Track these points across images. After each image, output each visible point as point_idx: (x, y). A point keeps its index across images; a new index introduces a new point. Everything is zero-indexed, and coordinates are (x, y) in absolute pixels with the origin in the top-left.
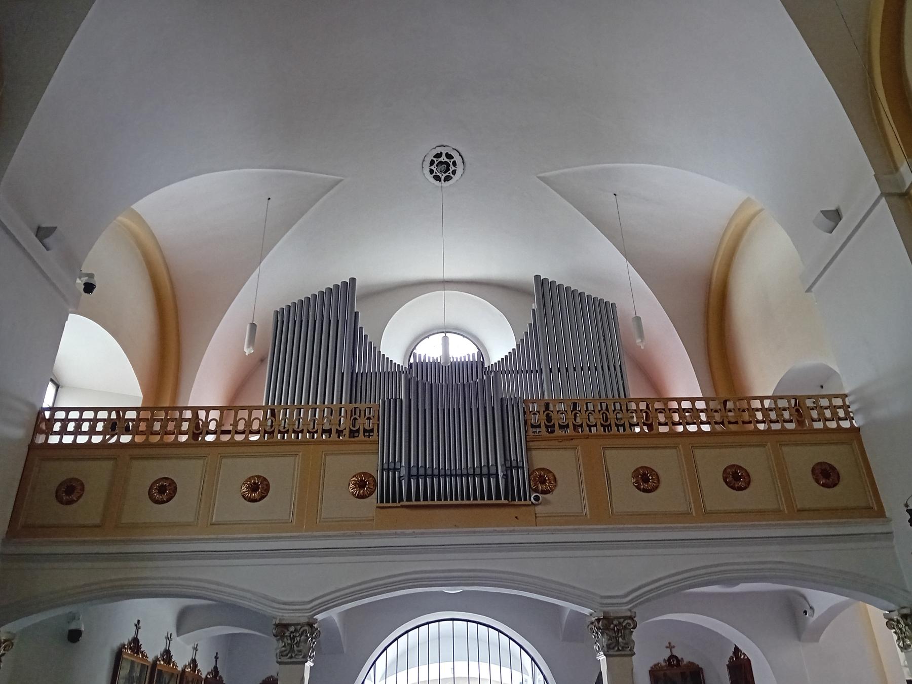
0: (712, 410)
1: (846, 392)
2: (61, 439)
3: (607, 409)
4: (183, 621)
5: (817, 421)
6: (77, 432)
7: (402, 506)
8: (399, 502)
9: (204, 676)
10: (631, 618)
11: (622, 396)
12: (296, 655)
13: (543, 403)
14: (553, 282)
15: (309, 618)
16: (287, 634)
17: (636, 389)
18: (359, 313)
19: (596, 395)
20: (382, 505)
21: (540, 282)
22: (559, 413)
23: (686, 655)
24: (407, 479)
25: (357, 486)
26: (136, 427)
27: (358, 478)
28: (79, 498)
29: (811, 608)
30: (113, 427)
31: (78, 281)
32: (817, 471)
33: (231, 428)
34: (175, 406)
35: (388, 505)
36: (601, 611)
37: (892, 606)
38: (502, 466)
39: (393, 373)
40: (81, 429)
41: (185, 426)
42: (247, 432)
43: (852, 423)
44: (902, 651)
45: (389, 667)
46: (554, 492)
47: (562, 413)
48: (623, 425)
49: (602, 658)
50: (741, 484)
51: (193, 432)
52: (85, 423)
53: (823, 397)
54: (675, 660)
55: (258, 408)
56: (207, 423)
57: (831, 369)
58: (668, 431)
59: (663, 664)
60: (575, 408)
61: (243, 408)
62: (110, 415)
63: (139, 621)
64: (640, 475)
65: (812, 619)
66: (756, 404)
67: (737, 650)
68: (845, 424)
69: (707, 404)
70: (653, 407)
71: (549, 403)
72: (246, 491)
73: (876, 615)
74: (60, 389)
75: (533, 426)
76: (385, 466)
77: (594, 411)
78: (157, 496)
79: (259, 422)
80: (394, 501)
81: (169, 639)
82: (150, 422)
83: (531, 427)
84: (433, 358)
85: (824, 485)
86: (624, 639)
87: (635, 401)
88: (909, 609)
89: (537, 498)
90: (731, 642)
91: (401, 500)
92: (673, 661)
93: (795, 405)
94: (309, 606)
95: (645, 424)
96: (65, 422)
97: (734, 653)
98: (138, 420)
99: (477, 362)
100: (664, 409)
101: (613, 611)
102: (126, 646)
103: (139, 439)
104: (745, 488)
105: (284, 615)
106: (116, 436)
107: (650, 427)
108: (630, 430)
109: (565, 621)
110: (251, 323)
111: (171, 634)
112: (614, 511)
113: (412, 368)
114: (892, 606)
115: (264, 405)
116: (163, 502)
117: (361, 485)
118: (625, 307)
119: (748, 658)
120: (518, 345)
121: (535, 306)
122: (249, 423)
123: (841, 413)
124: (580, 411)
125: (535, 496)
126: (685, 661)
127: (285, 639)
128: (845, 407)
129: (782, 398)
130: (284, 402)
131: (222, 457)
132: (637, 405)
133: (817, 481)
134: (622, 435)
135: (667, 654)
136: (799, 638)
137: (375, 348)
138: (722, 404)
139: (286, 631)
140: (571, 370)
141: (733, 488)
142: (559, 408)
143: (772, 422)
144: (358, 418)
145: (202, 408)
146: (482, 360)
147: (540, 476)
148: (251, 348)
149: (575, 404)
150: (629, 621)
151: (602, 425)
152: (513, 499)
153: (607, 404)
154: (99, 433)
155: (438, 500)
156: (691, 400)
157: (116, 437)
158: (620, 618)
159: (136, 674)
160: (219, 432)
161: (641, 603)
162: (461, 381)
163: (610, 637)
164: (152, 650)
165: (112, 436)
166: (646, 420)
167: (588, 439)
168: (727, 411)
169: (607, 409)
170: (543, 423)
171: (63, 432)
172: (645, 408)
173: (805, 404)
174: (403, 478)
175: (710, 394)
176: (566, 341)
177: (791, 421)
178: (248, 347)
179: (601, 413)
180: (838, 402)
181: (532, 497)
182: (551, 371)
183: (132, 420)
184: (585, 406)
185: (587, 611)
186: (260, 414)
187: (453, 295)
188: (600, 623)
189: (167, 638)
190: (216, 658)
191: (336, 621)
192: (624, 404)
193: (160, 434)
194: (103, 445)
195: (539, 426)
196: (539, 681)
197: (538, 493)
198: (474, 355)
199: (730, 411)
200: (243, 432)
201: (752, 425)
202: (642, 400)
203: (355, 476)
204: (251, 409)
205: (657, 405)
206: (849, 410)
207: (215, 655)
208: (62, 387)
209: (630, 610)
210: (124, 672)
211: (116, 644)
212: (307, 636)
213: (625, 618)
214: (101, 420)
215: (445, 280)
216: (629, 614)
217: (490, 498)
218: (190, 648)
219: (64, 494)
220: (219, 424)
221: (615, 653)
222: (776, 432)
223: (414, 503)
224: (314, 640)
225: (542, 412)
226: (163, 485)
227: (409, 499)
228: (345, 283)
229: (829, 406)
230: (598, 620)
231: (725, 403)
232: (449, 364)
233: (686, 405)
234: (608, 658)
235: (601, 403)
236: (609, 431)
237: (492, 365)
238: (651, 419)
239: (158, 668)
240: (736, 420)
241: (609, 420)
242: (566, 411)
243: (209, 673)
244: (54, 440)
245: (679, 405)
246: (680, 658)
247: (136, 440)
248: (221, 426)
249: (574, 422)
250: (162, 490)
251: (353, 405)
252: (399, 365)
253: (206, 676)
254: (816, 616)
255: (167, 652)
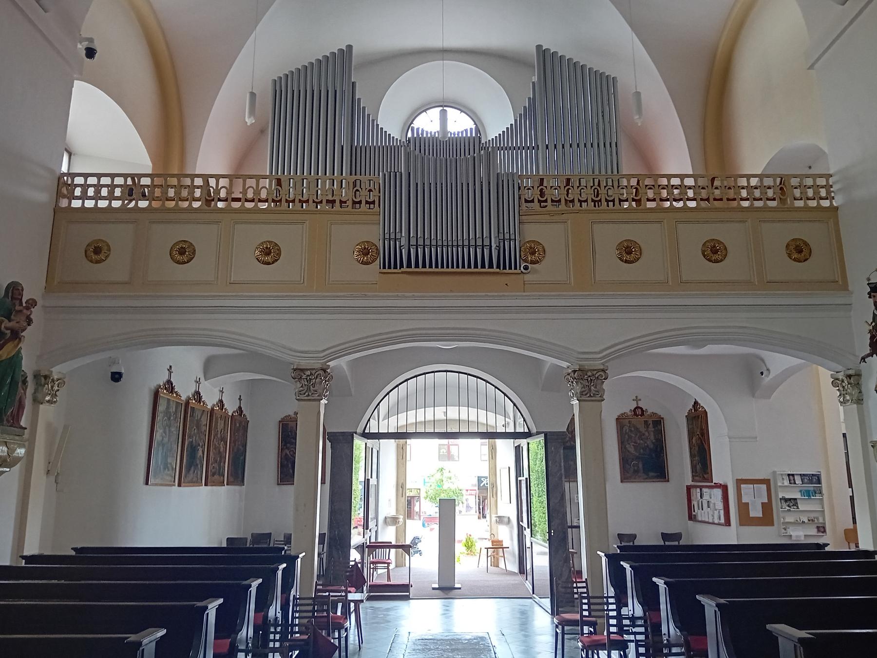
0: (699, 186)
1: (831, 172)
2: (83, 203)
3: (599, 185)
4: (210, 368)
5: (798, 200)
6: (97, 197)
7: (402, 273)
8: (400, 269)
9: (230, 414)
10: (603, 370)
11: (615, 172)
12: (313, 394)
13: (537, 179)
14: (555, 53)
15: (322, 365)
16: (304, 377)
17: (629, 166)
18: (357, 84)
19: (590, 170)
20: (384, 271)
21: (542, 53)
22: (553, 188)
23: (650, 407)
24: (407, 248)
25: (361, 253)
26: (152, 192)
27: (362, 247)
28: (107, 257)
29: (768, 370)
30: (130, 193)
31: (79, 46)
32: (791, 247)
33: (240, 196)
34: (184, 173)
35: (389, 271)
36: (577, 364)
37: (840, 368)
38: (495, 238)
39: (391, 150)
40: (100, 194)
41: (198, 193)
42: (256, 200)
43: (831, 203)
44: (841, 405)
45: (391, 409)
46: (543, 263)
47: (556, 189)
48: (613, 201)
49: (575, 402)
50: (714, 257)
51: (206, 198)
52: (77, 188)
53: (808, 176)
54: (640, 410)
55: (265, 177)
56: (217, 191)
57: (821, 150)
58: (655, 206)
59: (629, 413)
60: (568, 184)
61: (251, 177)
62: (126, 181)
63: (171, 367)
64: (624, 247)
65: (767, 380)
66: (743, 182)
67: (696, 403)
68: (826, 203)
69: (696, 181)
70: (643, 183)
71: (543, 179)
72: (260, 255)
73: (825, 375)
74: (72, 157)
75: (526, 201)
76: (387, 236)
77: (586, 187)
78: (179, 258)
79: (266, 191)
80: (395, 267)
81: (198, 382)
82: (165, 187)
83: (525, 202)
84: (431, 133)
85: (795, 260)
86: (596, 387)
87: (666, 176)
88: (854, 370)
89: (526, 268)
90: (692, 397)
91: (402, 266)
92: (639, 411)
93: (781, 184)
94: (322, 355)
95: (633, 200)
96: (85, 187)
97: (694, 406)
98: (153, 186)
99: (474, 137)
100: (653, 186)
101: (587, 364)
102: (162, 387)
103: (156, 204)
104: (721, 261)
105: (301, 361)
106: (134, 202)
107: (638, 202)
108: (619, 206)
109: (546, 370)
110: (250, 92)
111: (199, 379)
112: (597, 280)
113: (410, 143)
114: (840, 368)
115: (268, 174)
116: (184, 263)
117: (365, 252)
118: (626, 80)
119: (705, 410)
120: (516, 121)
121: (535, 79)
122: (257, 192)
123: (823, 192)
124: (573, 187)
125: (524, 266)
126: (650, 411)
127: (303, 382)
128: (828, 187)
129: (768, 176)
130: (287, 172)
131: (236, 223)
132: (629, 181)
133: (790, 256)
134: (612, 210)
135: (634, 405)
136: (753, 396)
137: (373, 121)
138: (710, 181)
139: (303, 375)
140: (567, 146)
141: (710, 260)
142: (552, 182)
143: (755, 199)
144: (360, 189)
145: (212, 176)
146: (479, 135)
147: (531, 248)
148: (252, 118)
149: (568, 180)
150: (602, 373)
151: (593, 200)
152: (505, 268)
153: (599, 180)
154: (117, 198)
155: (436, 267)
156: (666, 176)
157: (134, 202)
158: (594, 370)
159: (173, 409)
160: (229, 199)
161: (612, 359)
162: (455, 156)
163: (584, 386)
164: (185, 391)
165: (131, 201)
166: (636, 196)
167: (578, 214)
168: (714, 188)
169: (599, 185)
170: (537, 196)
171: (84, 197)
172: (635, 184)
173: (790, 183)
174: (403, 247)
175: (701, 172)
176: (572, 112)
177: (774, 199)
178: (249, 117)
179: (593, 188)
180: (822, 182)
181: (522, 266)
182: (547, 147)
183: (148, 186)
184: (605, 182)
185: (565, 364)
186: (266, 183)
187: (451, 65)
188: (576, 374)
189: (196, 382)
190: (240, 399)
191: (345, 369)
192: (616, 179)
193: (174, 201)
194: (123, 209)
195: (532, 201)
196: (519, 424)
197: (528, 263)
198: (471, 129)
199: (716, 188)
200: (253, 201)
201: (735, 202)
202: (633, 176)
203: (359, 244)
204: (258, 178)
205: (648, 182)
206: (832, 189)
207: (239, 397)
208: (74, 155)
209: (603, 364)
210: (162, 407)
211: (153, 385)
212: (321, 379)
213: (598, 371)
214: (118, 186)
215: (444, 49)
216: (602, 367)
217: (483, 266)
218: (216, 391)
219: (92, 254)
220: (229, 191)
221: (587, 399)
222: (759, 209)
223: (413, 269)
224: (327, 383)
225: (536, 188)
226: (182, 248)
227: (409, 265)
228: (341, 50)
229: (813, 186)
230: (574, 371)
231: (713, 180)
232: (447, 139)
233: (675, 181)
234: (582, 403)
235: (594, 179)
236: (599, 207)
237: (489, 140)
238: (640, 195)
239: (191, 405)
240: (721, 197)
241: (600, 195)
242: (560, 187)
243: (234, 412)
244: (76, 204)
245: (669, 181)
246: (644, 409)
247: (139, 206)
248: (231, 194)
249: (566, 197)
250: (182, 252)
251: (354, 177)
252: (397, 139)
253: (232, 414)
254: (771, 377)
255: (198, 393)
